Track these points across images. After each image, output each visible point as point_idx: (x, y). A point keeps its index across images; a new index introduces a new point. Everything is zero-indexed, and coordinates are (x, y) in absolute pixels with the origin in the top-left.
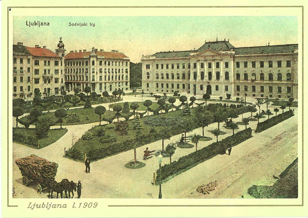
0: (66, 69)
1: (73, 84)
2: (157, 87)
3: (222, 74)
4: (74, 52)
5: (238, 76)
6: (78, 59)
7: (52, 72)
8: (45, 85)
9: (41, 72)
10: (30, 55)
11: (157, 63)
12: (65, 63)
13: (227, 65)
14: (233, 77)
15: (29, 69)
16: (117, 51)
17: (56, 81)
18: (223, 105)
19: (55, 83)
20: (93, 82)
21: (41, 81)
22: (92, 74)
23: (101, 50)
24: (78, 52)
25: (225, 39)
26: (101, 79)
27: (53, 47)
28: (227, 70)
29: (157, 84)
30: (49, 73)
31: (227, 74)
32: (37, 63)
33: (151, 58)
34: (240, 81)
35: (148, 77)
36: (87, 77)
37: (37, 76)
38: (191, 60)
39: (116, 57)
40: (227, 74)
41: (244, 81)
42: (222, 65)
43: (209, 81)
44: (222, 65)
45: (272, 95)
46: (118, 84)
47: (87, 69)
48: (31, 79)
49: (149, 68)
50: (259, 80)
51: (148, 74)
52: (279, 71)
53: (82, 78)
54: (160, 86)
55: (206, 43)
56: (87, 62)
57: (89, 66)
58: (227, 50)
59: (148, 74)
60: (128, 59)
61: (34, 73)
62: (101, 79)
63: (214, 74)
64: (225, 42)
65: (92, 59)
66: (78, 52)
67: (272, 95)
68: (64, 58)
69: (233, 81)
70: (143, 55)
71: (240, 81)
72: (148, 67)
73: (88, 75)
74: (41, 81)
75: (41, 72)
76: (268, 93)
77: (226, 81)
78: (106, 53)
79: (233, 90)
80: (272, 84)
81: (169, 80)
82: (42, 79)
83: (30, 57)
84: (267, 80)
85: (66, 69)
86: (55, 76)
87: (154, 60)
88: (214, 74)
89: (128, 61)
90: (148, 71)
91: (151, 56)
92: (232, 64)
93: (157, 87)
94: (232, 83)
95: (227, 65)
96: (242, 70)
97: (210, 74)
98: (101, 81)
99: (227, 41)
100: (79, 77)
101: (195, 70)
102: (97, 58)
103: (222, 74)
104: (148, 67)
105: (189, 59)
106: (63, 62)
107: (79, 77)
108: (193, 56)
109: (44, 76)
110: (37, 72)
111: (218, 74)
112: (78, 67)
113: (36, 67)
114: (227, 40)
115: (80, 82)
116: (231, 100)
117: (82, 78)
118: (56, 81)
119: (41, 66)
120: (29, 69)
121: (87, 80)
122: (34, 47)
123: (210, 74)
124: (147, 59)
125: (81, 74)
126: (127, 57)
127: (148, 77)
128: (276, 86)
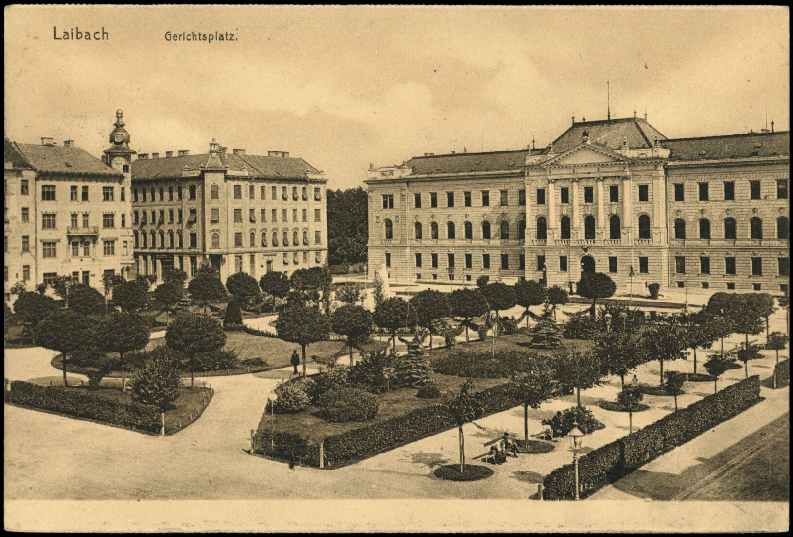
0: (136, 213)
1: (149, 258)
2: (419, 264)
3: (630, 222)
4: (150, 157)
5: (680, 227)
6: (165, 182)
7: (96, 221)
8: (76, 261)
9: (64, 223)
10: (27, 166)
11: (418, 188)
12: (135, 192)
13: (643, 194)
14: (663, 230)
15: (25, 210)
16: (283, 153)
17: (109, 247)
18: (647, 314)
19: (105, 254)
20: (215, 251)
21: (63, 248)
22: (209, 227)
23: (235, 150)
24: (162, 155)
25: (635, 113)
26: (238, 243)
27: (94, 142)
28: (644, 208)
29: (418, 256)
30: (86, 224)
31: (645, 222)
32: (49, 195)
33: (397, 174)
34: (737, 242)
35: (389, 236)
36: (193, 236)
37: (48, 235)
38: (527, 180)
39: (286, 174)
40: (645, 222)
41: (723, 242)
42: (629, 190)
43: (586, 244)
44: (629, 190)
45: (760, 285)
46: (290, 255)
47: (193, 212)
48: (32, 243)
49: (392, 206)
50: (748, 240)
51: (389, 224)
52: (702, 211)
53: (176, 238)
54: (427, 260)
55: (576, 125)
56: (193, 190)
57: (198, 199)
58: (644, 147)
59: (389, 224)
60: (318, 177)
61: (40, 224)
62: (238, 243)
63: (603, 223)
64: (633, 120)
65: (210, 179)
66: (162, 155)
67: (760, 285)
68: (128, 177)
69: (664, 243)
70: (371, 166)
71: (763, 242)
72: (388, 202)
73: (197, 228)
74: (63, 248)
75: (64, 223)
76: (777, 277)
77: (612, 244)
78: (250, 161)
79: (665, 273)
80: (473, 247)
81: (457, 242)
82: (65, 241)
83: (29, 175)
84: (774, 240)
85: (136, 213)
86: (105, 234)
87: (408, 181)
88: (603, 223)
89: (320, 186)
90: (389, 214)
91: (399, 168)
92: (660, 188)
93: (419, 264)
94: (660, 248)
95: (643, 194)
96: (691, 210)
97: (590, 222)
98: (239, 249)
99: (643, 117)
100: (167, 237)
101: (541, 210)
102: (227, 178)
103: (630, 222)
104: (388, 202)
105: (522, 175)
106: (128, 191)
107: (167, 237)
108: (538, 167)
109: (74, 233)
110: (49, 221)
111: (616, 223)
112: (173, 205)
113: (48, 207)
114: (640, 116)
115: (161, 250)
116: (660, 300)
117: (176, 238)
118: (109, 247)
119: (64, 206)
120: (25, 210)
121: (194, 244)
122: (40, 142)
123: (590, 222)
124: (384, 178)
125: (175, 228)
126: (319, 173)
127: (389, 236)
128: (748, 255)
